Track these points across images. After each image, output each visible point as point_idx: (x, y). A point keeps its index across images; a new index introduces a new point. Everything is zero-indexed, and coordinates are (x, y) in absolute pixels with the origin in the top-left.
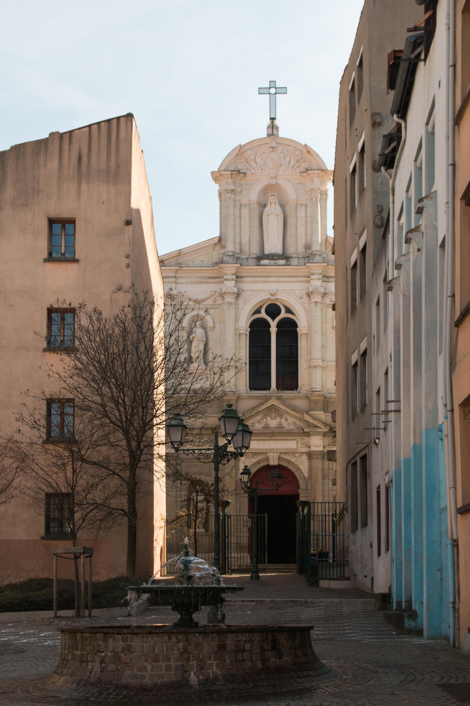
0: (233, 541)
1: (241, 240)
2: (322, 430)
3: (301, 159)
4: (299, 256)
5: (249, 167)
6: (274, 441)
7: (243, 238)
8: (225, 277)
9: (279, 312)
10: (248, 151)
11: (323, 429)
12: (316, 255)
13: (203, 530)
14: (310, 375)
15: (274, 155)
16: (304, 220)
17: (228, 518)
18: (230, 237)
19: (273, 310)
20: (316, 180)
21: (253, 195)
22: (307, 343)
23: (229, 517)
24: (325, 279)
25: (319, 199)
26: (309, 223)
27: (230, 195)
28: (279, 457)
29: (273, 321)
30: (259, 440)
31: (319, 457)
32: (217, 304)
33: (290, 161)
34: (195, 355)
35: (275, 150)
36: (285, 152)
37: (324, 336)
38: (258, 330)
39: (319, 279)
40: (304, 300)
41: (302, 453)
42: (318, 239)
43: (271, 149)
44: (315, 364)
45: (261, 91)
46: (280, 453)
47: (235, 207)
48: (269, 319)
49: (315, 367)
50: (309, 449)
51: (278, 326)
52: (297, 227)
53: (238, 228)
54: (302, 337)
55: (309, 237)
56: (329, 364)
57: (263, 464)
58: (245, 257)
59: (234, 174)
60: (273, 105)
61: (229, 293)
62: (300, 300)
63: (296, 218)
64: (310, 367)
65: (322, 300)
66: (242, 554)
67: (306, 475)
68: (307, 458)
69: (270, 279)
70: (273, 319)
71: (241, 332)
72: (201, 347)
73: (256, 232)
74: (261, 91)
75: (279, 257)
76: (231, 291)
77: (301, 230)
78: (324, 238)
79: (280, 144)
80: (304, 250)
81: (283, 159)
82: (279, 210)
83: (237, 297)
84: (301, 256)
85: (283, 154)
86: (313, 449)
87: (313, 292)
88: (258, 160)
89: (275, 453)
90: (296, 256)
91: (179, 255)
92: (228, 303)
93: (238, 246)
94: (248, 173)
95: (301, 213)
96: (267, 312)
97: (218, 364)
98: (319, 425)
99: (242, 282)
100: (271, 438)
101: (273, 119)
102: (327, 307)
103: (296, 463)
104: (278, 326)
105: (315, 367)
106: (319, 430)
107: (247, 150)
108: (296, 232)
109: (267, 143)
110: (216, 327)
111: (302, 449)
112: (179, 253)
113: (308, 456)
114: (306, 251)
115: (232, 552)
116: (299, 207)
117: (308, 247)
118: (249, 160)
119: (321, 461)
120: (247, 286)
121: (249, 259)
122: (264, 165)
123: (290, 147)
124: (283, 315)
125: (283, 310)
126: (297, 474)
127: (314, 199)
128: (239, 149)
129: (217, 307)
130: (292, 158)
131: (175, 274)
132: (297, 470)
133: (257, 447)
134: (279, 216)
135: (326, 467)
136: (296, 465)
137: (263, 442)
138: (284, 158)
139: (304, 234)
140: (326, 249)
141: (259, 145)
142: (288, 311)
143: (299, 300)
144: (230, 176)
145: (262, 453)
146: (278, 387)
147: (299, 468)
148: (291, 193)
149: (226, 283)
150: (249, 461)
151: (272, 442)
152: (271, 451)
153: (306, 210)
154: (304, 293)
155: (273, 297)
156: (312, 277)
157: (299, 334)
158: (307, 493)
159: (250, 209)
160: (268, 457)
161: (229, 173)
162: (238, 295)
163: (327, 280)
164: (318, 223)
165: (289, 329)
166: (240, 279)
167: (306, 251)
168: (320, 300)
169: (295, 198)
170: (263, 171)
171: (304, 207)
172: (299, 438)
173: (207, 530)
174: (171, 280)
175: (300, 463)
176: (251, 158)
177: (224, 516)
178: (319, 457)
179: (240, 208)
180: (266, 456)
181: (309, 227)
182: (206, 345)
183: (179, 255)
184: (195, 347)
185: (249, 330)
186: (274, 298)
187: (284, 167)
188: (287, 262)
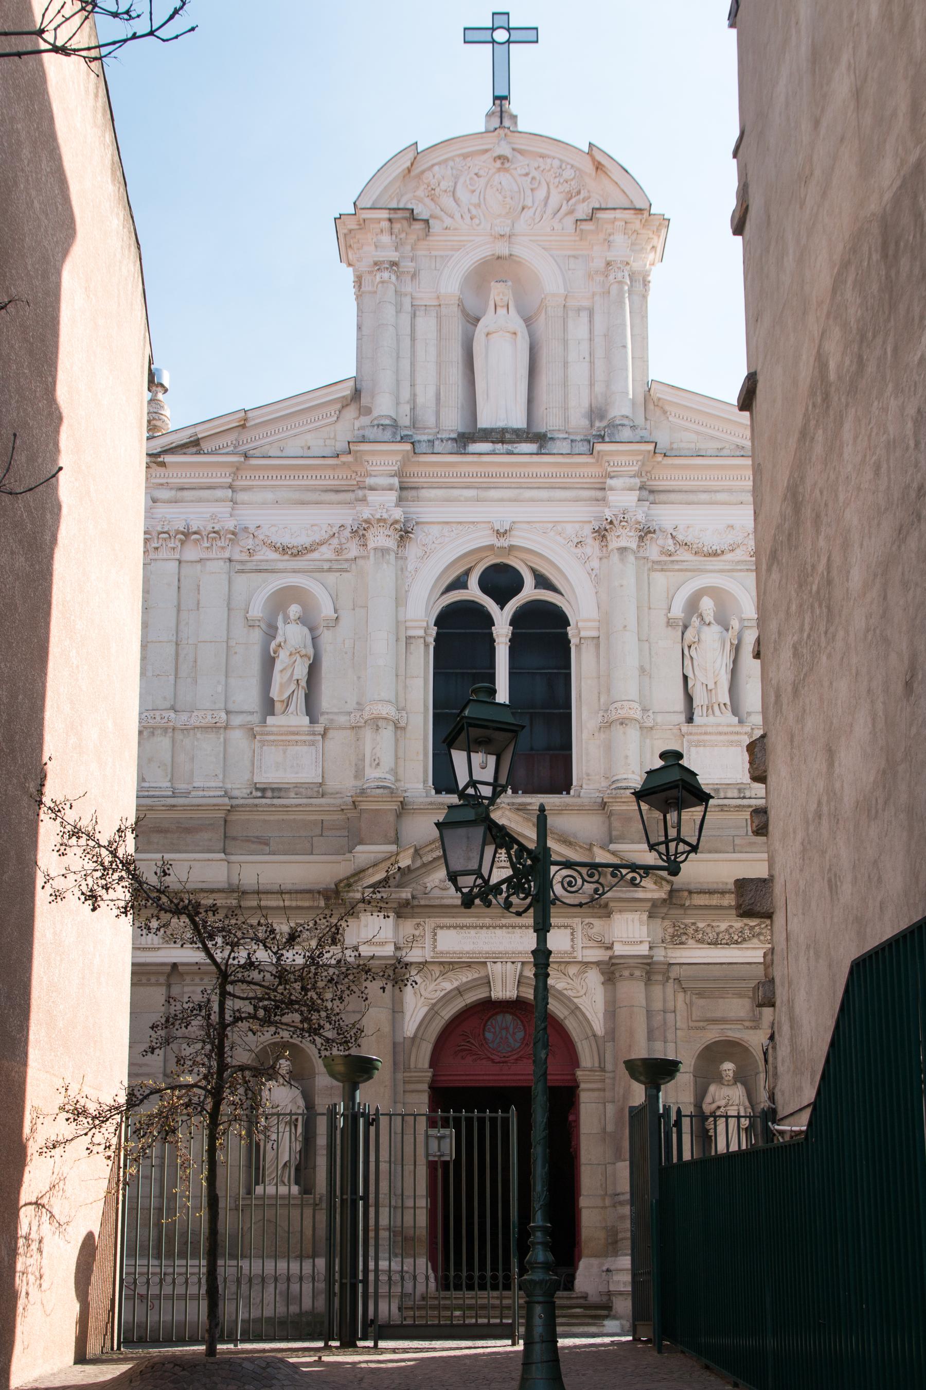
0: (384, 1221)
1: (414, 396)
2: (649, 895)
3: (579, 193)
4: (572, 437)
5: (438, 212)
6: (504, 930)
7: (419, 390)
8: (370, 481)
9: (517, 585)
10: (436, 168)
11: (653, 891)
12: (623, 425)
13: (295, 1189)
14: (608, 748)
15: (504, 179)
16: (585, 346)
17: (368, 1124)
18: (386, 380)
19: (501, 581)
20: (619, 239)
21: (449, 281)
22: (598, 662)
23: (372, 1121)
24: (645, 493)
25: (626, 288)
26: (599, 353)
27: (386, 275)
28: (521, 975)
29: (502, 609)
30: (462, 927)
31: (637, 973)
32: (347, 560)
33: (547, 198)
34: (281, 692)
35: (507, 165)
36: (534, 173)
37: (646, 645)
38: (458, 635)
39: (631, 489)
40: (588, 550)
41: (586, 964)
42: (626, 386)
43: (498, 164)
44: (623, 713)
45: (471, 36)
46: (523, 963)
47: (399, 311)
48: (490, 604)
49: (623, 722)
50: (609, 953)
51: (515, 621)
52: (566, 364)
53: (406, 364)
54: (584, 647)
55: (599, 388)
56: (659, 719)
57: (472, 997)
58: (425, 438)
59: (398, 220)
60: (501, 70)
61: (379, 520)
62: (578, 551)
63: (565, 342)
64: (607, 725)
65: (639, 546)
66: (409, 1261)
67: (599, 1026)
68: (601, 979)
69: (493, 494)
70: (502, 604)
71: (411, 633)
72: (301, 671)
73: (455, 373)
74: (471, 36)
75: (518, 436)
76: (385, 516)
77: (579, 373)
78: (641, 391)
79: (520, 152)
80: (585, 422)
81: (529, 192)
82: (515, 322)
83: (401, 537)
84: (578, 438)
85: (529, 179)
86: (619, 950)
87: (615, 522)
88: (461, 193)
89: (509, 964)
90: (566, 436)
91: (243, 426)
92: (375, 549)
93: (406, 409)
94: (435, 225)
95: (579, 329)
96: (486, 586)
97: (347, 718)
99: (418, 499)
100: (498, 922)
101: (500, 99)
102: (651, 570)
103: (569, 993)
104: (514, 622)
105: (623, 722)
107: (433, 166)
108: (566, 377)
109: (486, 151)
110: (343, 622)
111: (587, 952)
112: (243, 422)
113: (603, 974)
114: (592, 426)
115: (384, 1254)
116: (570, 314)
117: (596, 413)
118: (438, 190)
119: (642, 984)
120: (430, 509)
121: (437, 443)
122: (479, 205)
123: (549, 161)
124: (529, 592)
125: (529, 580)
126: (571, 1025)
127: (614, 289)
128: (411, 155)
129: (345, 566)
130: (551, 187)
131: (230, 480)
132: (572, 1012)
133: (457, 948)
134: (519, 334)
135: (658, 1005)
136: (569, 998)
137: (473, 932)
138: (532, 190)
139: (587, 382)
140: (646, 419)
141: (465, 156)
142: (542, 582)
143: (574, 550)
144: (385, 225)
145: (469, 965)
147: (577, 1008)
148: (549, 274)
149: (372, 497)
150: (432, 986)
151: (498, 932)
152: (497, 957)
153: (591, 321)
154: (587, 530)
155: (502, 540)
156: (610, 482)
157: (574, 642)
158: (603, 1081)
159: (439, 317)
160: (487, 976)
161: (385, 215)
162: (405, 534)
163: (651, 498)
164: (625, 347)
165: (546, 634)
166: (413, 493)
167: (592, 426)
168: (634, 546)
169: (562, 291)
170: (476, 221)
171: (584, 316)
172: (578, 920)
173: (307, 1189)
174: (219, 493)
175: (582, 993)
176: (444, 185)
177: (353, 1117)
178: (637, 973)
179: (414, 316)
180: (483, 974)
181: (599, 364)
182: (313, 670)
183: (243, 426)
184: (281, 671)
185: (434, 631)
186: (504, 542)
187: (532, 211)
188: (541, 447)
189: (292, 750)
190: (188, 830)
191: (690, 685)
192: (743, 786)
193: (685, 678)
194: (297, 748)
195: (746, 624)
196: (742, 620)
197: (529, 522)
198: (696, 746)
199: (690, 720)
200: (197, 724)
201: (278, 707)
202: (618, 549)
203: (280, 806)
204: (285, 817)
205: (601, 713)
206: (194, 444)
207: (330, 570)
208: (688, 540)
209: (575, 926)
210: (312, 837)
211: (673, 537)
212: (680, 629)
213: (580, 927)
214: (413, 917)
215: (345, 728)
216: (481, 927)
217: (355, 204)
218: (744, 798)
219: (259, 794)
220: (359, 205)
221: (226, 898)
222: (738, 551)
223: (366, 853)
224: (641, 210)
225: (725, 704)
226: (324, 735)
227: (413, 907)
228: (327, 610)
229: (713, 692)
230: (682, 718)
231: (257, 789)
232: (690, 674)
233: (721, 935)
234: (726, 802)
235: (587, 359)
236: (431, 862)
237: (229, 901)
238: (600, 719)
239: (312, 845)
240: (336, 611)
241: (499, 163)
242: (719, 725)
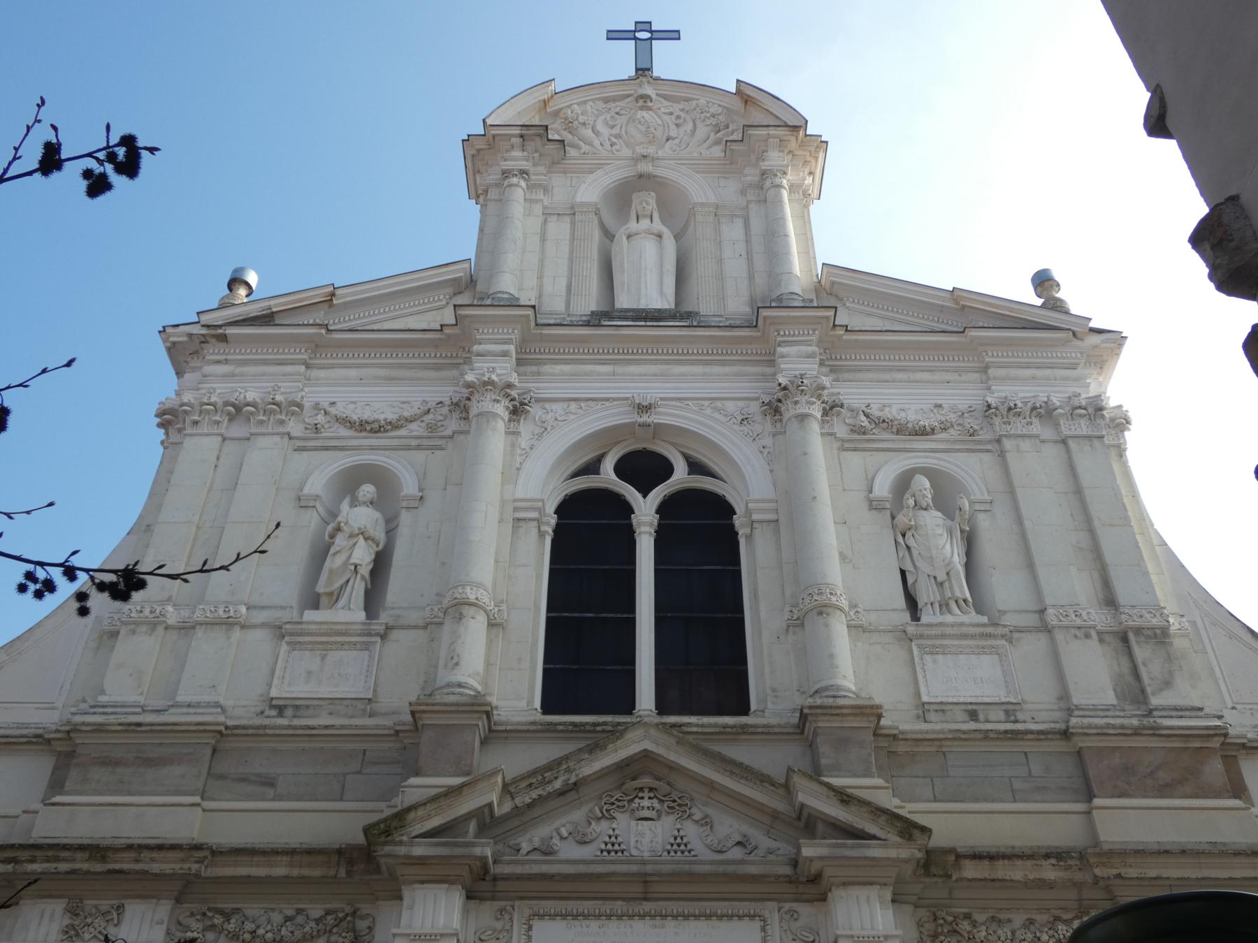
2: (892, 853)
9: (665, 469)
19: (644, 468)
22: (779, 548)
29: (645, 497)
30: (575, 917)
32: (442, 437)
38: (586, 535)
48: (630, 492)
51: (662, 509)
54: (757, 533)
55: (760, 280)
85: (673, 117)
87: (791, 388)
98: (872, 829)
106: (875, 851)
124: (680, 477)
129: (439, 442)
134: (665, 236)
137: (594, 925)
142: (696, 467)
143: (736, 427)
146: (663, 706)
148: (699, 189)
151: (638, 924)
154: (754, 407)
157: (742, 532)
159: (573, 224)
165: (704, 531)
189: (334, 656)
190: (151, 763)
191: (910, 580)
192: (1011, 707)
193: (903, 573)
194: (343, 653)
195: (977, 507)
196: (971, 503)
197: (679, 399)
198: (932, 653)
199: (915, 617)
200: (201, 619)
201: (324, 600)
202: (797, 416)
203: (302, 727)
204: (307, 745)
205: (788, 609)
206: (267, 319)
207: (418, 448)
208: (887, 414)
209: (767, 914)
210: (345, 775)
211: (867, 416)
212: (888, 513)
213: (776, 916)
214: (493, 899)
215: (416, 627)
216: (609, 917)
217: (484, 121)
218: (1016, 721)
219: (274, 713)
220: (489, 122)
221: (183, 860)
222: (951, 431)
223: (420, 786)
224: (796, 127)
225: (965, 601)
226: (383, 637)
227: (495, 879)
228: (409, 486)
229: (947, 585)
230: (907, 616)
231: (272, 707)
232: (908, 567)
233: (1018, 933)
234: (989, 726)
235: (744, 256)
236: (530, 806)
237: (186, 866)
238: (787, 615)
239: (343, 787)
240: (421, 490)
241: (641, 103)
242: (962, 624)
